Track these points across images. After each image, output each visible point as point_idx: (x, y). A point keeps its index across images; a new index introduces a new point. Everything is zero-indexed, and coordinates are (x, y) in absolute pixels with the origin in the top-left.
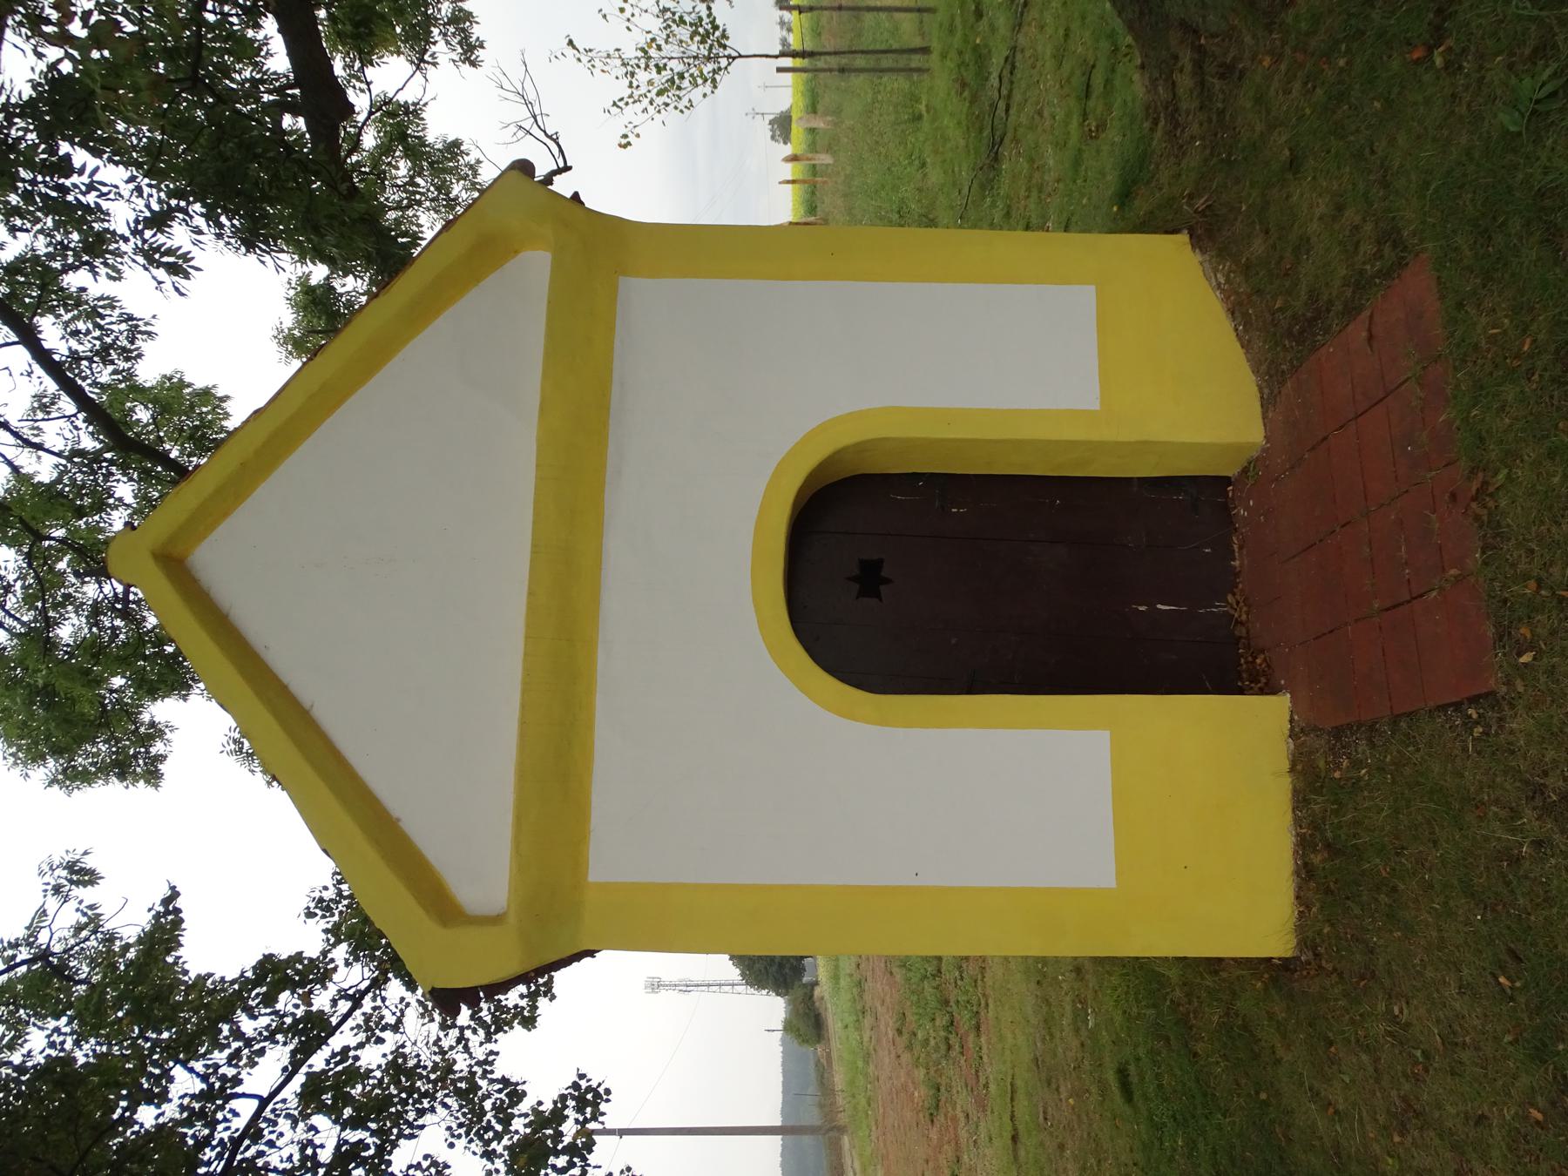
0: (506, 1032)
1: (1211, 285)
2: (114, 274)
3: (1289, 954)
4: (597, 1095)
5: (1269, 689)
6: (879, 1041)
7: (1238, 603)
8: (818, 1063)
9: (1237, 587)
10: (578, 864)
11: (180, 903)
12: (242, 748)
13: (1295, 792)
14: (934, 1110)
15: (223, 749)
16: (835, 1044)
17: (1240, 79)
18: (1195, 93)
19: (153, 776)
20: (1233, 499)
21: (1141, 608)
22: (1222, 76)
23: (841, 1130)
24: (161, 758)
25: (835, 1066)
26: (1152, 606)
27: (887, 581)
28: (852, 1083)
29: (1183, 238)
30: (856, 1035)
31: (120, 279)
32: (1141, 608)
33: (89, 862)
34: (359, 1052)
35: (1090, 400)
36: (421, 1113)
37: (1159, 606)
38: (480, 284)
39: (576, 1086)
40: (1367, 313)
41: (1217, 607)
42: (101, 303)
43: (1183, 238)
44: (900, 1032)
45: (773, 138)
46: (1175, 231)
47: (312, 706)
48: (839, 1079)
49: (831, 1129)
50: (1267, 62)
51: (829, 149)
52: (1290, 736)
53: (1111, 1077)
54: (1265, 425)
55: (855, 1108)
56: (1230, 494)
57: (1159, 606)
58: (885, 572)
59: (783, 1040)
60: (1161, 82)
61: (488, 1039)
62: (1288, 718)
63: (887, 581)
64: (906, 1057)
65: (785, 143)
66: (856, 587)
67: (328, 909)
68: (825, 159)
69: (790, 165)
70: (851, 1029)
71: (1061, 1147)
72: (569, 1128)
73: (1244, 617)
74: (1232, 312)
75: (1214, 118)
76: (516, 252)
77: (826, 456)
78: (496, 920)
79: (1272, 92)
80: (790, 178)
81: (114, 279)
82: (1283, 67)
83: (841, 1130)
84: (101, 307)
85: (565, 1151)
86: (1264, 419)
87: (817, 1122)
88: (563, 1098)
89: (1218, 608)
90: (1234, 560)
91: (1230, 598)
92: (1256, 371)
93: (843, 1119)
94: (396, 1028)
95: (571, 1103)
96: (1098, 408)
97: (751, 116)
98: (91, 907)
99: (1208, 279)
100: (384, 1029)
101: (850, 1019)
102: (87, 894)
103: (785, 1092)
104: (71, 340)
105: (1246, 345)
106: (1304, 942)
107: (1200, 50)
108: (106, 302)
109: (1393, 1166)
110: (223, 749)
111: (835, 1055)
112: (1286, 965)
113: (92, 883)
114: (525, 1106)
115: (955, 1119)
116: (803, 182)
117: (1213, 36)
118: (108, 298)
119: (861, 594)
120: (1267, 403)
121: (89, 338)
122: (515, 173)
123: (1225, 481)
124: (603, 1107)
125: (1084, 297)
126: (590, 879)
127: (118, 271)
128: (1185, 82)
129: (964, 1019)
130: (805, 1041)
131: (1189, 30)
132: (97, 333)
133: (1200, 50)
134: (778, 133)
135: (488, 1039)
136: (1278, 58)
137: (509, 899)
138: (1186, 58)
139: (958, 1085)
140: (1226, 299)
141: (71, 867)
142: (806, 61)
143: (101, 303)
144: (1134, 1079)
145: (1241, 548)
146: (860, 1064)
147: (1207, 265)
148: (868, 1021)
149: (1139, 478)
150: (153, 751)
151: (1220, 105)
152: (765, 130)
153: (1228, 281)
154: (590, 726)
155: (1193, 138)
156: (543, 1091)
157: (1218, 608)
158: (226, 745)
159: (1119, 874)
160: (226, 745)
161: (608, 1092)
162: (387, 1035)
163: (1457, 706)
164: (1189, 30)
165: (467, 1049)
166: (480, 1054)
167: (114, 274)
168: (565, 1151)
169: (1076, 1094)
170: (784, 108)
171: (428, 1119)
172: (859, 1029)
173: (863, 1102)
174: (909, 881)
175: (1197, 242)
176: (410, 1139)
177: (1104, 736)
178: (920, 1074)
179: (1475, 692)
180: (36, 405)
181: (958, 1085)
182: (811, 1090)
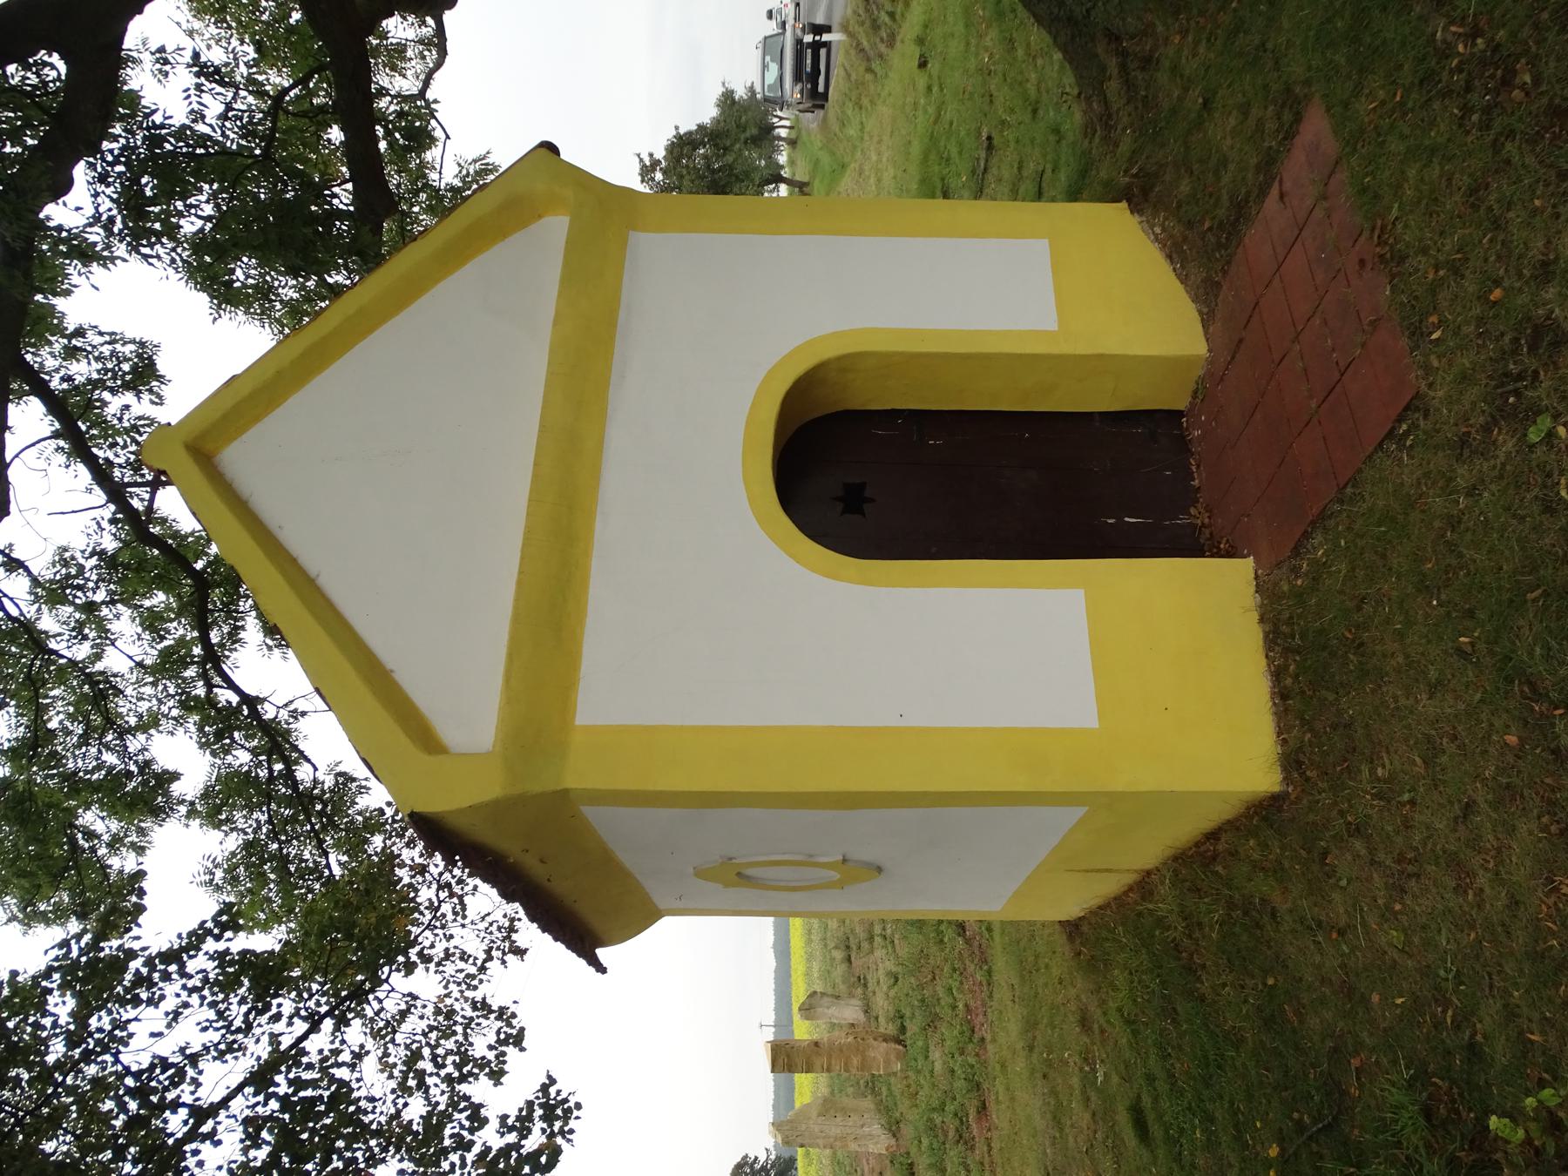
0: (470, 1083)
1: (1149, 238)
2: (157, 400)
3: (1277, 789)
7: (1200, 513)
9: (1198, 502)
12: (213, 880)
13: (1266, 636)
15: (193, 879)
17: (1157, 64)
18: (1123, 92)
20: (1187, 429)
21: (1110, 521)
22: (1143, 69)
26: (1120, 519)
31: (162, 404)
32: (1110, 521)
35: (1048, 321)
37: (1127, 519)
38: (507, 240)
40: (1278, 179)
41: (1181, 519)
42: (142, 422)
43: (1124, 205)
46: (1119, 201)
47: (318, 576)
50: (1177, 39)
52: (1257, 592)
53: (1123, 1119)
54: (1207, 340)
56: (1185, 425)
57: (1127, 519)
58: (868, 493)
60: (1095, 98)
62: (1253, 576)
63: (872, 500)
66: (840, 506)
73: (1207, 521)
74: (1170, 257)
75: (1140, 105)
76: (540, 217)
77: (811, 366)
79: (1184, 60)
81: (157, 404)
82: (1190, 38)
84: (143, 426)
86: (1205, 336)
88: (530, 1104)
89: (1183, 520)
90: (1194, 480)
91: (1193, 511)
92: (1195, 300)
95: (539, 1112)
96: (1056, 329)
99: (1147, 234)
104: (108, 451)
105: (1184, 279)
107: (1124, 54)
108: (146, 422)
109: (1398, 938)
110: (193, 879)
117: (1132, 38)
118: (148, 418)
120: (1206, 324)
121: (125, 451)
122: (543, 151)
123: (1180, 414)
125: (1039, 248)
126: (577, 722)
127: (159, 397)
128: (1113, 87)
131: (1114, 37)
132: (133, 448)
133: (1124, 54)
136: (1184, 33)
137: (495, 741)
138: (1113, 64)
140: (1163, 246)
143: (142, 422)
144: (1151, 1117)
145: (1198, 466)
147: (1145, 224)
149: (1100, 413)
151: (1143, 93)
153: (1164, 230)
155: (1124, 129)
157: (1183, 520)
158: (197, 875)
159: (1101, 715)
160: (197, 875)
161: (578, 1106)
163: (1390, 434)
164: (1114, 37)
167: (157, 400)
174: (893, 721)
175: (1135, 209)
176: (445, 53)
179: (1404, 404)
180: (57, 558)
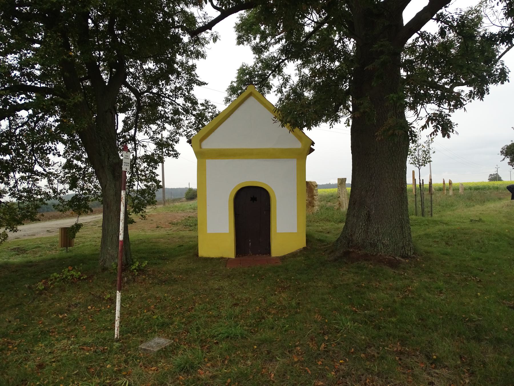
4: (177, 157)
5: (236, 257)
6: (187, 213)
8: (180, 199)
10: (208, 158)
11: (205, 85)
14: (172, 223)
16: (186, 203)
19: (239, 43)
23: (164, 204)
24: (243, 44)
25: (181, 203)
27: (253, 202)
28: (176, 207)
29: (305, 246)
30: (188, 207)
33: (218, 40)
34: (181, 105)
36: (173, 125)
39: (178, 153)
43: (305, 246)
44: (189, 217)
45: (491, 175)
48: (177, 204)
49: (164, 202)
51: (454, 194)
55: (170, 208)
59: (187, 188)
61: (185, 135)
63: (253, 202)
64: (183, 218)
65: (489, 179)
67: (206, 104)
68: (451, 193)
69: (448, 182)
70: (190, 207)
71: (169, 240)
72: (172, 153)
78: (201, 147)
80: (433, 183)
83: (164, 204)
85: (168, 152)
87: (166, 198)
88: (176, 151)
93: (167, 205)
94: (187, 119)
97: (496, 167)
98: (209, 42)
100: (186, 117)
101: (192, 206)
102: (212, 41)
103: (172, 189)
106: (200, 257)
111: (183, 203)
112: (197, 255)
113: (214, 42)
114: (174, 143)
115: (171, 227)
116: (444, 187)
119: (251, 198)
124: (175, 158)
129: (191, 228)
130: (187, 194)
134: (493, 177)
135: (185, 135)
139: (178, 227)
141: (217, 37)
142: (419, 186)
146: (181, 209)
148: (192, 210)
150: (245, 42)
152: (493, 172)
154: (228, 159)
156: (177, 147)
162: (185, 118)
165: (183, 131)
166: (183, 134)
168: (168, 152)
169: (178, 241)
170: (502, 179)
171: (172, 126)
172: (190, 209)
173: (172, 210)
175: (304, 248)
177: (228, 232)
178: (180, 221)
181: (178, 227)
182: (173, 197)
